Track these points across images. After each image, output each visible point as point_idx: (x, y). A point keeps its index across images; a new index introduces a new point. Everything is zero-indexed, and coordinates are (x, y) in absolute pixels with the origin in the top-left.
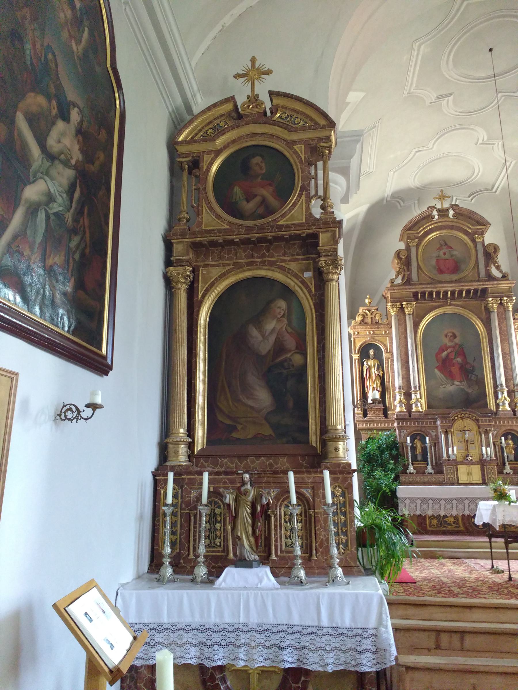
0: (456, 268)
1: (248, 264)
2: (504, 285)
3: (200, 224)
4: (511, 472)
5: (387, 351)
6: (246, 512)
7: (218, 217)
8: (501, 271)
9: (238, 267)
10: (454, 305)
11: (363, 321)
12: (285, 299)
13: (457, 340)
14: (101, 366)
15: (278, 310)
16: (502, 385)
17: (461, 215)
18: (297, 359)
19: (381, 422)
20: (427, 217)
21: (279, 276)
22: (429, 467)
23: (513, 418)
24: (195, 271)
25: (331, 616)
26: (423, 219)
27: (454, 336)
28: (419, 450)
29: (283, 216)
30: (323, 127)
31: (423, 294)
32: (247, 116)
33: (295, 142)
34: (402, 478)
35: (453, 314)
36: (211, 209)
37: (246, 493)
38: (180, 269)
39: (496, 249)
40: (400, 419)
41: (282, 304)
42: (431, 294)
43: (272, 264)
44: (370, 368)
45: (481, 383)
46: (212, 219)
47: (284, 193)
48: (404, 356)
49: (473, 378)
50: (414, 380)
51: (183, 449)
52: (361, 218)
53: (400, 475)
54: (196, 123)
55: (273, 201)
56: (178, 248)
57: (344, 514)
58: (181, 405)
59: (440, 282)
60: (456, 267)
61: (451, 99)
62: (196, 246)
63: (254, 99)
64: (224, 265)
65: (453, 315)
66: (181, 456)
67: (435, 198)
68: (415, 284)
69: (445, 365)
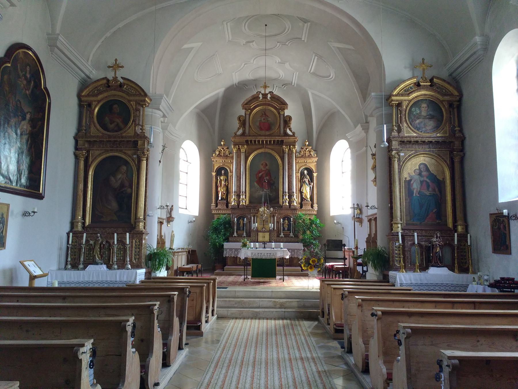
0: (269, 128)
1: (111, 150)
2: (291, 139)
3: (90, 133)
4: (283, 236)
5: (230, 172)
6: (97, 248)
7: (98, 130)
8: (291, 131)
9: (107, 151)
10: (267, 148)
11: (219, 154)
12: (126, 165)
14: (40, 197)
15: (122, 170)
16: (286, 192)
17: (274, 98)
18: (129, 190)
20: (255, 98)
21: (123, 156)
22: (245, 233)
24: (88, 152)
26: (254, 98)
27: (266, 165)
28: (241, 225)
29: (125, 132)
30: (142, 96)
31: (251, 141)
32: (112, 86)
33: (131, 101)
34: (230, 239)
36: (95, 126)
37: (99, 240)
38: (80, 152)
39: (290, 118)
40: (233, 208)
41: (124, 168)
42: (255, 141)
43: (121, 151)
44: (221, 180)
46: (96, 130)
47: (126, 122)
48: (238, 175)
49: (274, 188)
50: (243, 189)
52: (221, 95)
53: (325, 242)
55: (121, 125)
56: (80, 142)
57: (139, 248)
58: (80, 208)
59: (260, 135)
62: (89, 142)
63: (115, 79)
64: (101, 150)
65: (265, 153)
66: (80, 228)
67: (261, 87)
68: (246, 136)
69: (260, 181)
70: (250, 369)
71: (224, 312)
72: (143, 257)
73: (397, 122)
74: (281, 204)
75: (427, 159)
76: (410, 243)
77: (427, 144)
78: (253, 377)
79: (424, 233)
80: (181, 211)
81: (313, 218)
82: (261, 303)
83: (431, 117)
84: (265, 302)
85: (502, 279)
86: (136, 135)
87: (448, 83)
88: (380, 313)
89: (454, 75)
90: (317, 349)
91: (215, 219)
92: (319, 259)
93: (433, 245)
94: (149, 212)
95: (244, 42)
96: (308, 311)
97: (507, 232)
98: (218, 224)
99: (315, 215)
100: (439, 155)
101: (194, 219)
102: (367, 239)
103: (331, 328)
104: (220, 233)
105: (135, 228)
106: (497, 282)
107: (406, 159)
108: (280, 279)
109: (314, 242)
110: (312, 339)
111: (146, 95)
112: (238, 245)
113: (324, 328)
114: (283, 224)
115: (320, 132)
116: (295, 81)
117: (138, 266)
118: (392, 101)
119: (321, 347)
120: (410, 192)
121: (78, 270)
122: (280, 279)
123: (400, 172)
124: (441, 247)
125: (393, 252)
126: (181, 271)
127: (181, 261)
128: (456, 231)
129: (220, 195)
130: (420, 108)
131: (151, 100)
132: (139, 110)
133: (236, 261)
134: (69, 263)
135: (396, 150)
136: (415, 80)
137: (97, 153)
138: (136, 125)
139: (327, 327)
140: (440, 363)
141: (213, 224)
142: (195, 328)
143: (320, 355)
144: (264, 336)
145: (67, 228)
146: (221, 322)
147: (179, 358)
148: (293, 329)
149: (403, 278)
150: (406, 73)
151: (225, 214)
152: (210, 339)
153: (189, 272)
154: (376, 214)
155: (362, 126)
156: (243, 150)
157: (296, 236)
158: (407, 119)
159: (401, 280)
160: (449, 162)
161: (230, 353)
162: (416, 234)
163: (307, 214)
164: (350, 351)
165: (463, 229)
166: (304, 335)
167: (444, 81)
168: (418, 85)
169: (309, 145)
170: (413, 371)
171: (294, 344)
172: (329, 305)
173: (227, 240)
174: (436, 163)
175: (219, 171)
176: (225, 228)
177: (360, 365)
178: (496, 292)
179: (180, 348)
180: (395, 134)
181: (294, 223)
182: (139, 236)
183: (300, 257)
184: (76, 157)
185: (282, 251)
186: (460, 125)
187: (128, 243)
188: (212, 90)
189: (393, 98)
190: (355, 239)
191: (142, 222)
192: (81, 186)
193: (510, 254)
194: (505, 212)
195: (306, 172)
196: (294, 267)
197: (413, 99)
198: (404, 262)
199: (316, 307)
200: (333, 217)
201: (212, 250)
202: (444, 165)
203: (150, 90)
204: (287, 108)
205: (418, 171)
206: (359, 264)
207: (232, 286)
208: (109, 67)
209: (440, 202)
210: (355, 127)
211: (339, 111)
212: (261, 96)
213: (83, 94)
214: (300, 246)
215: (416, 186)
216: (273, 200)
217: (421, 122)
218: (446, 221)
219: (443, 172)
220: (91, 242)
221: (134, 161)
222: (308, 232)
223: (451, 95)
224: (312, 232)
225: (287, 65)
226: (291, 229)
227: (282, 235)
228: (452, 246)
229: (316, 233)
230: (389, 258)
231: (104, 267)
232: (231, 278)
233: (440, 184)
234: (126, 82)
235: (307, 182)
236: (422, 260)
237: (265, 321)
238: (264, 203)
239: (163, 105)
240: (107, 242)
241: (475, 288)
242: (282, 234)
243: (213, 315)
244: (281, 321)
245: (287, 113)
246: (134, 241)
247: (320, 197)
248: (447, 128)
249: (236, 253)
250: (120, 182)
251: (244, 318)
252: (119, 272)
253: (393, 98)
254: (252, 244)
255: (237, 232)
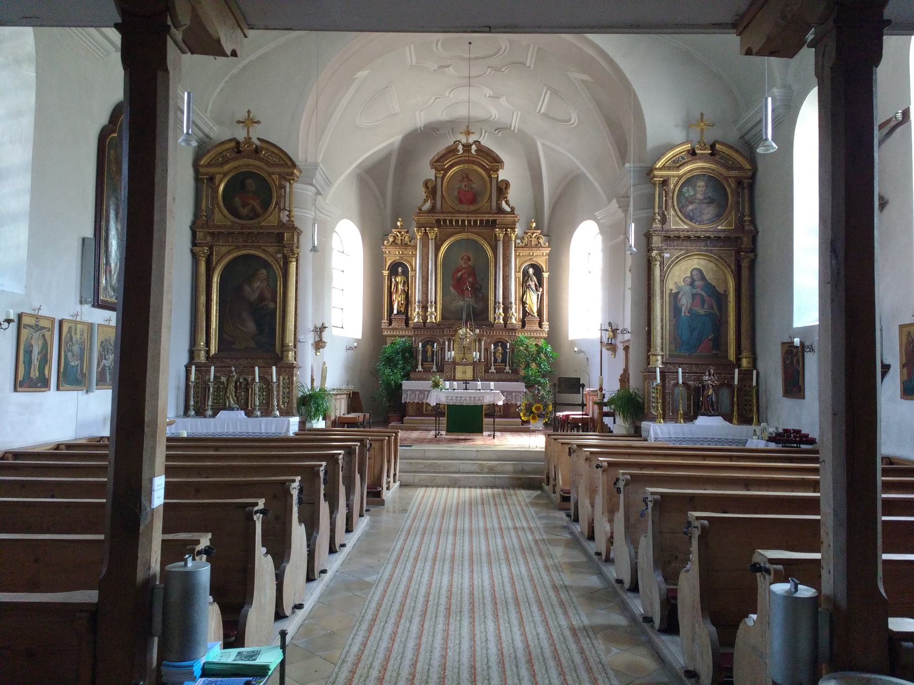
1: (244, 246)
2: (509, 218)
3: (213, 221)
5: (412, 270)
6: (232, 386)
7: (225, 217)
9: (238, 248)
11: (394, 242)
12: (265, 269)
13: (470, 263)
17: (482, 151)
19: (401, 329)
20: (452, 151)
22: (434, 367)
23: (501, 329)
24: (211, 248)
25: (266, 429)
27: (469, 259)
28: (429, 353)
29: (264, 220)
33: (273, 173)
34: (412, 375)
35: (468, 240)
36: (220, 211)
37: (233, 376)
38: (200, 249)
39: (507, 184)
40: (416, 328)
41: (264, 272)
42: (451, 221)
43: (258, 247)
44: (397, 283)
45: (486, 300)
46: (222, 217)
47: (266, 205)
48: (425, 273)
49: (480, 295)
51: (203, 353)
52: (396, 145)
54: (212, 153)
55: (258, 209)
56: (200, 235)
59: (460, 212)
60: (473, 199)
61: (451, 68)
62: (212, 234)
63: (248, 140)
66: (202, 358)
68: (438, 213)
69: (459, 284)
70: (451, 537)
71: (408, 477)
72: (295, 401)
73: (660, 207)
74: (492, 320)
75: (703, 262)
76: (673, 382)
77: (704, 240)
78: (454, 544)
79: (694, 369)
80: (336, 332)
81: (542, 343)
82: (462, 467)
83: (711, 201)
84: (468, 465)
85: (785, 431)
86: (281, 224)
87: (737, 151)
88: (605, 464)
89: (747, 137)
90: (536, 520)
91: (388, 345)
92: (546, 406)
93: (704, 386)
94: (301, 337)
95: (436, 67)
96: (528, 477)
97: (800, 369)
98: (393, 352)
99: (545, 339)
100: (720, 257)
101: (356, 344)
102: (621, 376)
103: (556, 497)
104: (396, 366)
105: (281, 359)
106: (778, 434)
107: (672, 262)
108: (489, 435)
109: (542, 381)
110: (531, 509)
111: (294, 165)
112: (426, 385)
113: (549, 497)
114: (495, 353)
115: (557, 204)
116: (515, 124)
117: (287, 413)
118: (655, 177)
119: (541, 518)
120: (676, 310)
121: (205, 417)
122: (489, 435)
123: (662, 281)
124: (716, 389)
125: (649, 396)
126: (340, 423)
127: (339, 408)
128: (739, 365)
129: (395, 306)
130: (694, 187)
131: (301, 172)
132: (284, 187)
133: (421, 409)
134: (191, 408)
135: (658, 249)
136: (688, 146)
137: (224, 250)
138: (280, 210)
139: (553, 495)
140: (645, 500)
141: (385, 352)
142: (375, 494)
143: (539, 525)
144: (467, 506)
145: (185, 359)
146: (407, 492)
147: (362, 525)
148: (506, 498)
149: (659, 431)
150: (677, 135)
151: (402, 336)
152: (391, 509)
153: (352, 424)
154: (628, 341)
155: (618, 202)
156: (431, 235)
157: (515, 371)
158: (675, 203)
159: (656, 433)
160: (733, 267)
161: (423, 521)
162: (680, 370)
163: (532, 337)
164: (576, 520)
165: (749, 363)
166: (521, 505)
167: (730, 147)
168: (692, 153)
169: (536, 228)
170: (632, 521)
171: (507, 513)
172: (555, 467)
173: (407, 377)
174: (715, 268)
175: (394, 269)
176: (404, 359)
177: (586, 532)
178: (779, 447)
179: (361, 515)
180: (657, 225)
181: (513, 351)
182: (288, 370)
183: (519, 403)
184: (194, 256)
185: (492, 393)
186: (752, 214)
187: (275, 380)
188: (383, 138)
189: (656, 173)
190: (604, 377)
191: (291, 350)
192: (203, 299)
193: (804, 398)
194: (797, 341)
195: (531, 271)
196: (508, 417)
197: (685, 174)
198: (663, 410)
199: (540, 472)
200: (573, 343)
201: (385, 393)
202: (726, 271)
203: (299, 157)
204: (502, 167)
205: (689, 280)
206: (607, 414)
207: (416, 443)
208: (239, 122)
209: (719, 324)
210: (610, 202)
211: (584, 174)
212: (460, 147)
213: (202, 163)
214: (520, 386)
215: (685, 302)
216: (479, 316)
217: (696, 208)
218: (727, 351)
219: (726, 281)
220: (223, 379)
221: (279, 263)
222: (533, 365)
223: (741, 168)
224: (539, 365)
225: (503, 100)
226: (506, 361)
227: (493, 370)
228: (730, 386)
229: (545, 366)
230: (644, 404)
231: (242, 413)
232: (415, 434)
233: (720, 298)
234: (264, 145)
235: (533, 287)
236: (689, 406)
237: (467, 490)
238: (467, 322)
239: (318, 179)
240: (245, 379)
241: (757, 443)
242: (493, 367)
243: (394, 482)
244: (489, 490)
245: (502, 175)
246: (281, 378)
247: (553, 311)
248: (733, 217)
249: (421, 396)
250: (258, 292)
251: (438, 487)
252: (264, 419)
253: (656, 173)
254: (447, 383)
255: (422, 365)
